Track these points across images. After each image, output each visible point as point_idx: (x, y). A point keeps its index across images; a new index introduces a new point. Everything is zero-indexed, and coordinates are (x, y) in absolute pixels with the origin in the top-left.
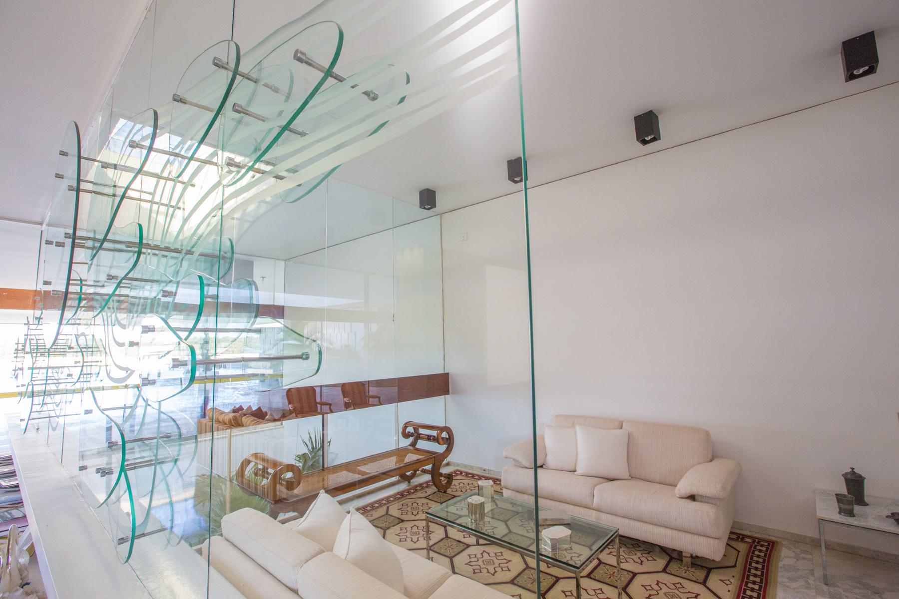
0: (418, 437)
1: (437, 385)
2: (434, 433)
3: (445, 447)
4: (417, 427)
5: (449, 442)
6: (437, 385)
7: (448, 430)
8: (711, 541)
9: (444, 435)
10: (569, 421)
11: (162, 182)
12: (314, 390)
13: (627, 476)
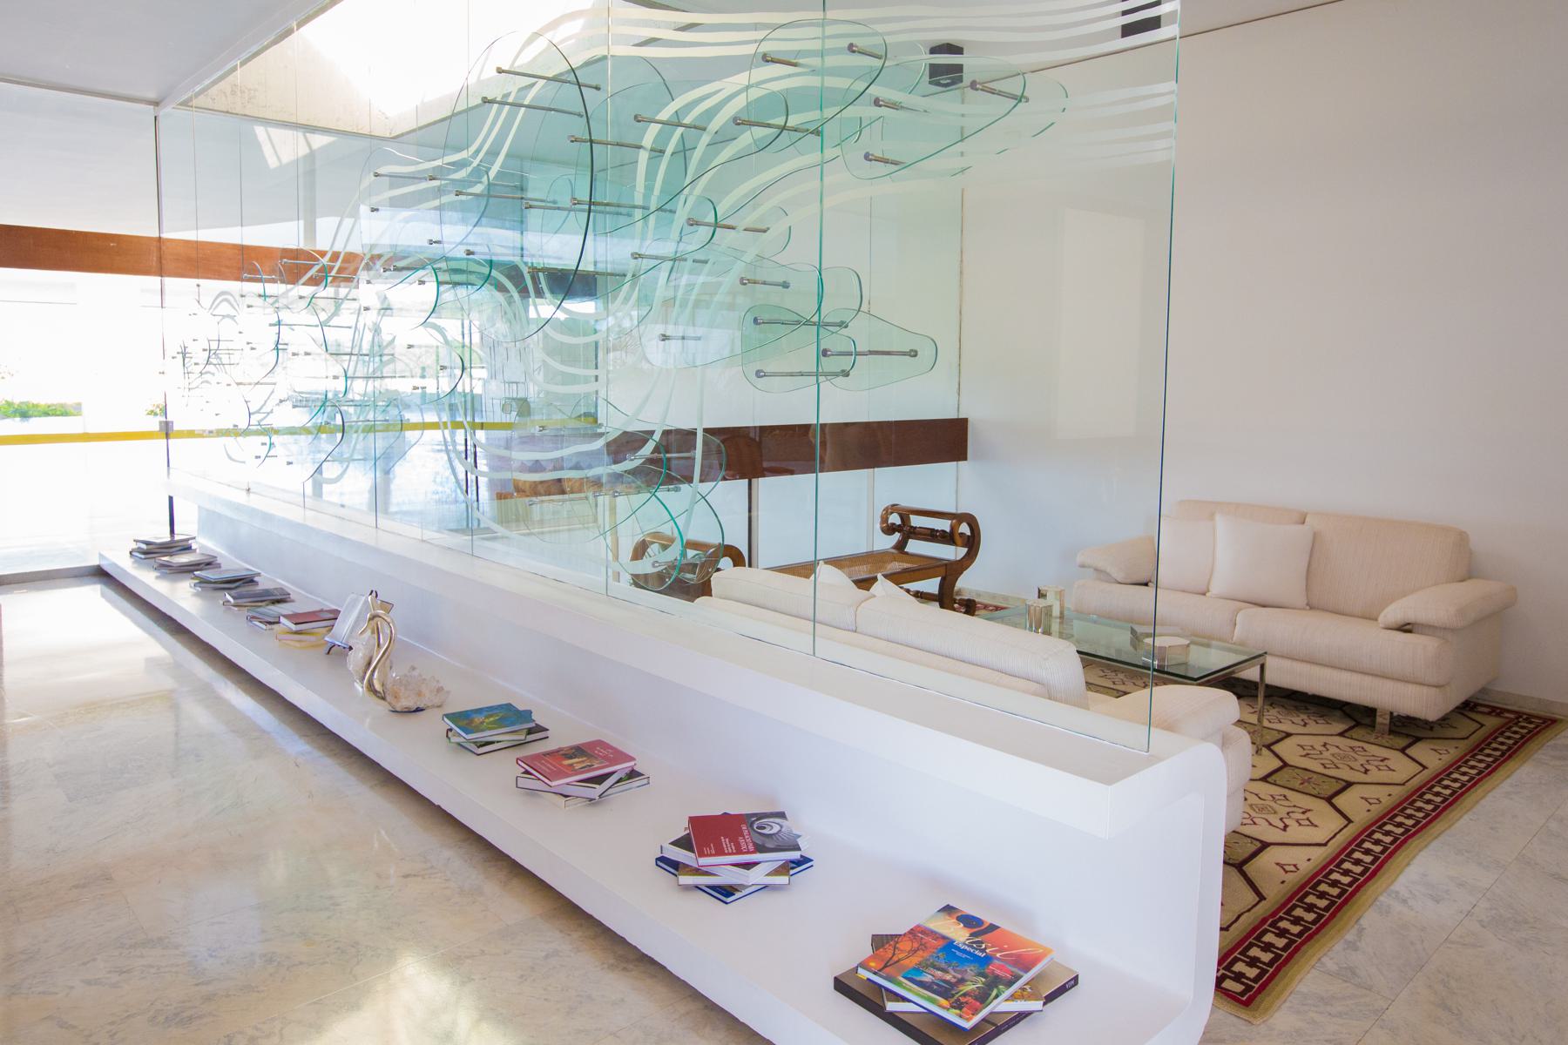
0: (909, 533)
1: (943, 440)
2: (944, 525)
3: (962, 551)
4: (905, 514)
5: (972, 543)
6: (943, 440)
7: (971, 520)
8: (1425, 690)
9: (964, 529)
10: (1206, 510)
11: (356, 351)
12: (688, 451)
13: (1302, 601)
